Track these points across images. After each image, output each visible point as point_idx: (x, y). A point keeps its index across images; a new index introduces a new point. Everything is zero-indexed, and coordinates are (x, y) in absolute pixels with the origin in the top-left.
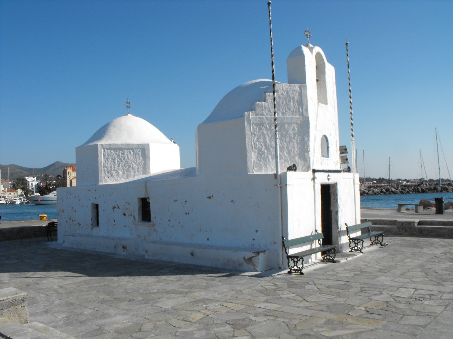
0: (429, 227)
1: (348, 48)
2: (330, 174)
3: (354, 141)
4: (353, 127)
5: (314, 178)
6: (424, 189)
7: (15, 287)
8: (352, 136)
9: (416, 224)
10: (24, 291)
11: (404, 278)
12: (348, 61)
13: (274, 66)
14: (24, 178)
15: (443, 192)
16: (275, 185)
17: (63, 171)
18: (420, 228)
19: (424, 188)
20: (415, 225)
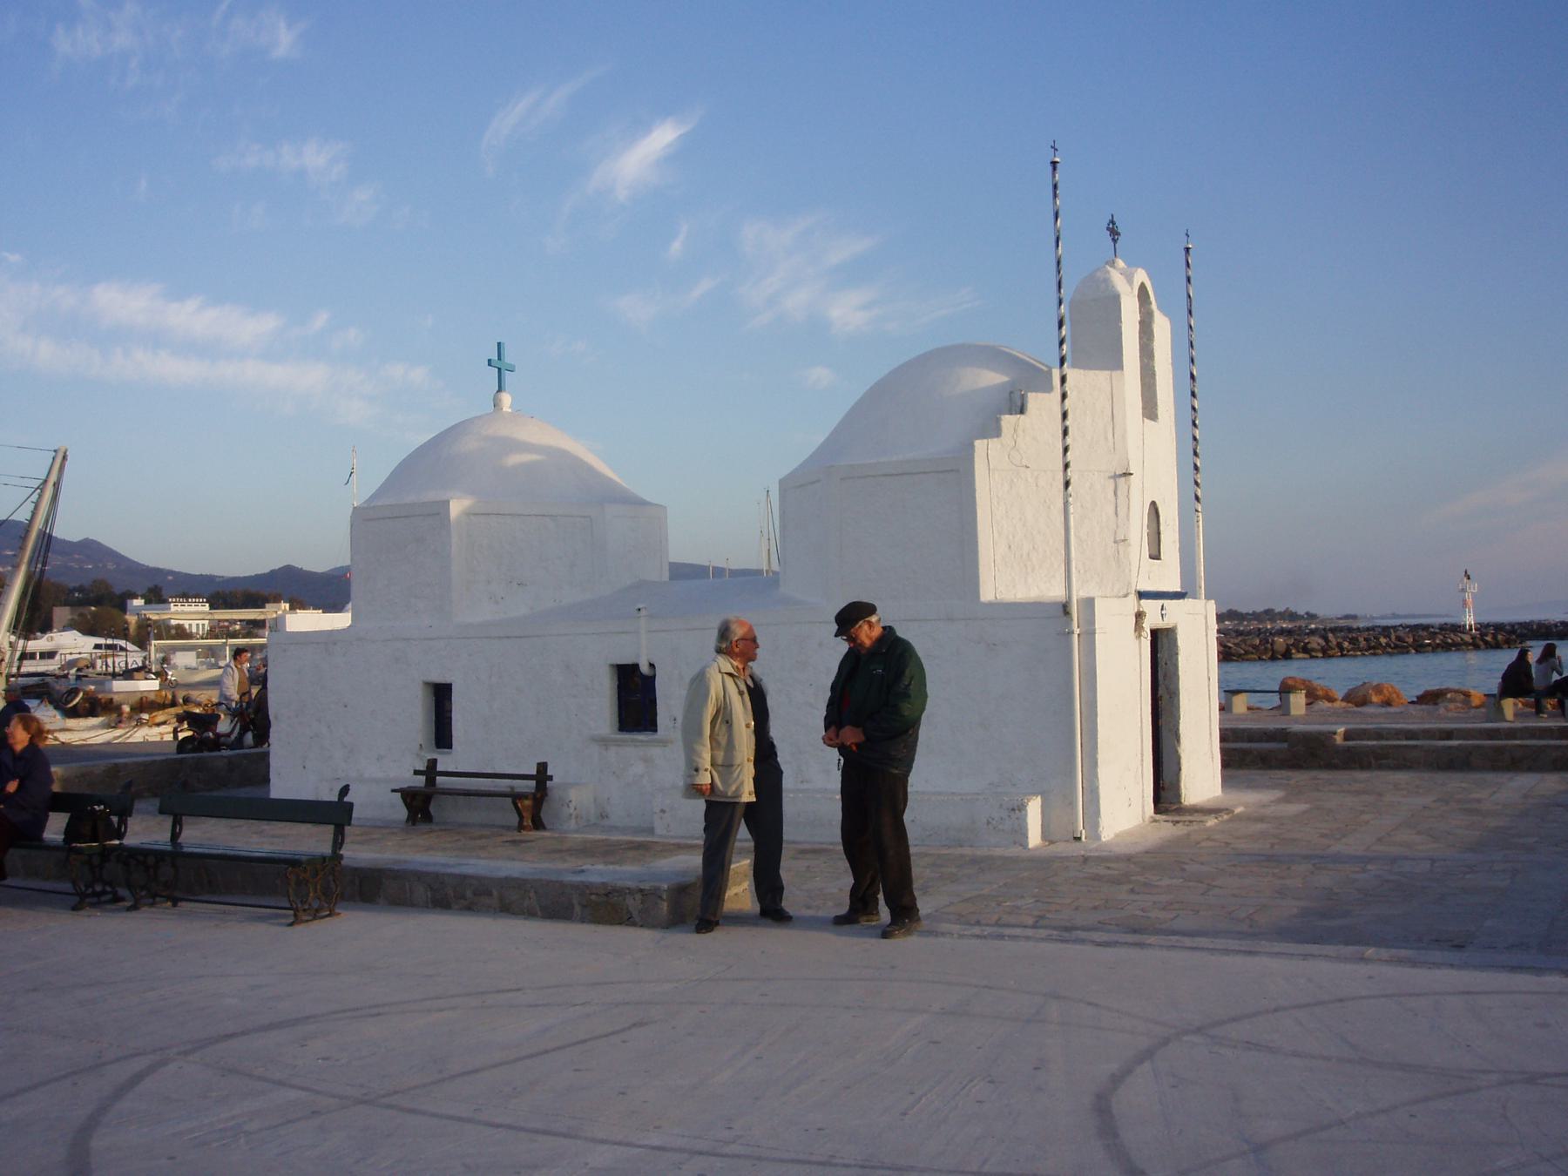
0: (1373, 746)
1: (1190, 261)
2: (1166, 602)
3: (1200, 514)
4: (1199, 476)
5: (1140, 616)
6: (1230, 645)
7: (1306, 803)
8: (1197, 498)
9: (1339, 739)
10: (1136, 843)
11: (1099, 944)
12: (1189, 296)
13: (1062, 307)
14: (349, 606)
15: (1291, 658)
16: (868, 633)
17: (1293, 609)
18: (1349, 749)
19: (1229, 642)
20: (1335, 740)
